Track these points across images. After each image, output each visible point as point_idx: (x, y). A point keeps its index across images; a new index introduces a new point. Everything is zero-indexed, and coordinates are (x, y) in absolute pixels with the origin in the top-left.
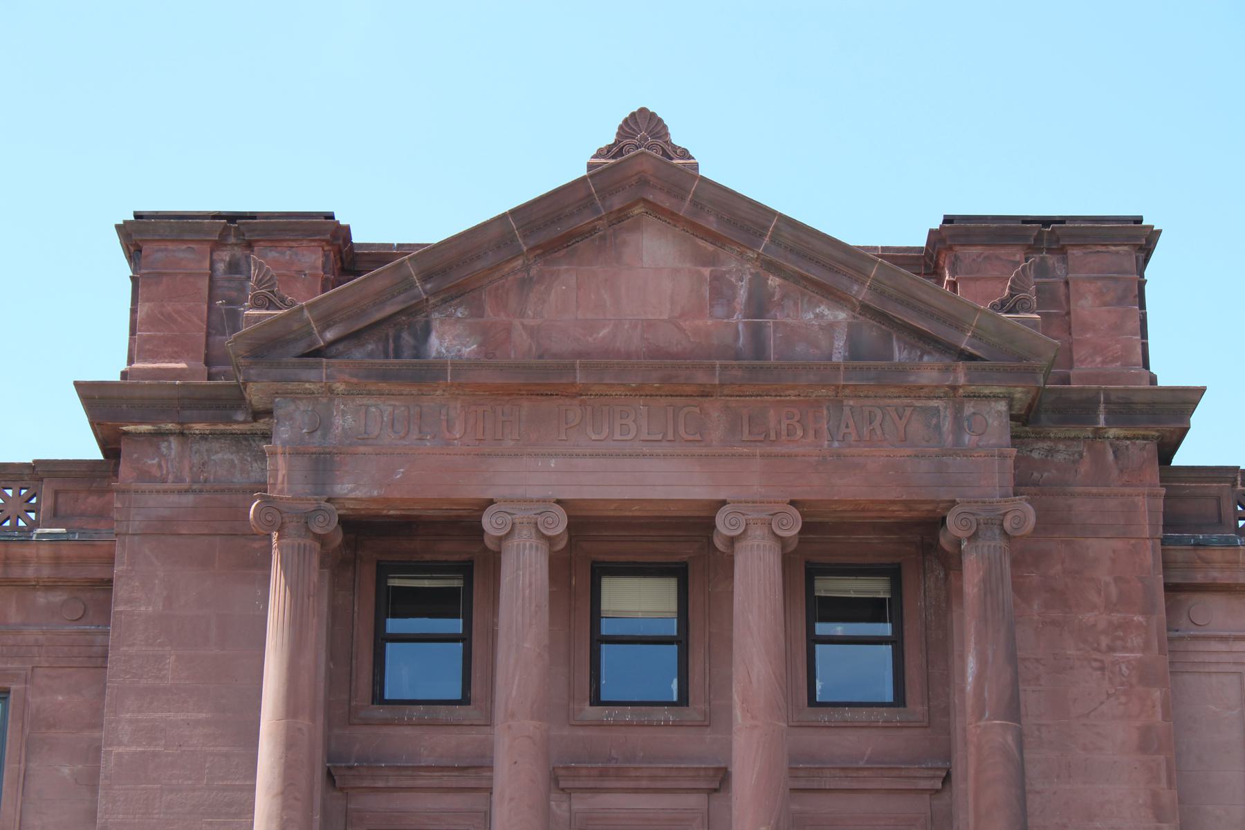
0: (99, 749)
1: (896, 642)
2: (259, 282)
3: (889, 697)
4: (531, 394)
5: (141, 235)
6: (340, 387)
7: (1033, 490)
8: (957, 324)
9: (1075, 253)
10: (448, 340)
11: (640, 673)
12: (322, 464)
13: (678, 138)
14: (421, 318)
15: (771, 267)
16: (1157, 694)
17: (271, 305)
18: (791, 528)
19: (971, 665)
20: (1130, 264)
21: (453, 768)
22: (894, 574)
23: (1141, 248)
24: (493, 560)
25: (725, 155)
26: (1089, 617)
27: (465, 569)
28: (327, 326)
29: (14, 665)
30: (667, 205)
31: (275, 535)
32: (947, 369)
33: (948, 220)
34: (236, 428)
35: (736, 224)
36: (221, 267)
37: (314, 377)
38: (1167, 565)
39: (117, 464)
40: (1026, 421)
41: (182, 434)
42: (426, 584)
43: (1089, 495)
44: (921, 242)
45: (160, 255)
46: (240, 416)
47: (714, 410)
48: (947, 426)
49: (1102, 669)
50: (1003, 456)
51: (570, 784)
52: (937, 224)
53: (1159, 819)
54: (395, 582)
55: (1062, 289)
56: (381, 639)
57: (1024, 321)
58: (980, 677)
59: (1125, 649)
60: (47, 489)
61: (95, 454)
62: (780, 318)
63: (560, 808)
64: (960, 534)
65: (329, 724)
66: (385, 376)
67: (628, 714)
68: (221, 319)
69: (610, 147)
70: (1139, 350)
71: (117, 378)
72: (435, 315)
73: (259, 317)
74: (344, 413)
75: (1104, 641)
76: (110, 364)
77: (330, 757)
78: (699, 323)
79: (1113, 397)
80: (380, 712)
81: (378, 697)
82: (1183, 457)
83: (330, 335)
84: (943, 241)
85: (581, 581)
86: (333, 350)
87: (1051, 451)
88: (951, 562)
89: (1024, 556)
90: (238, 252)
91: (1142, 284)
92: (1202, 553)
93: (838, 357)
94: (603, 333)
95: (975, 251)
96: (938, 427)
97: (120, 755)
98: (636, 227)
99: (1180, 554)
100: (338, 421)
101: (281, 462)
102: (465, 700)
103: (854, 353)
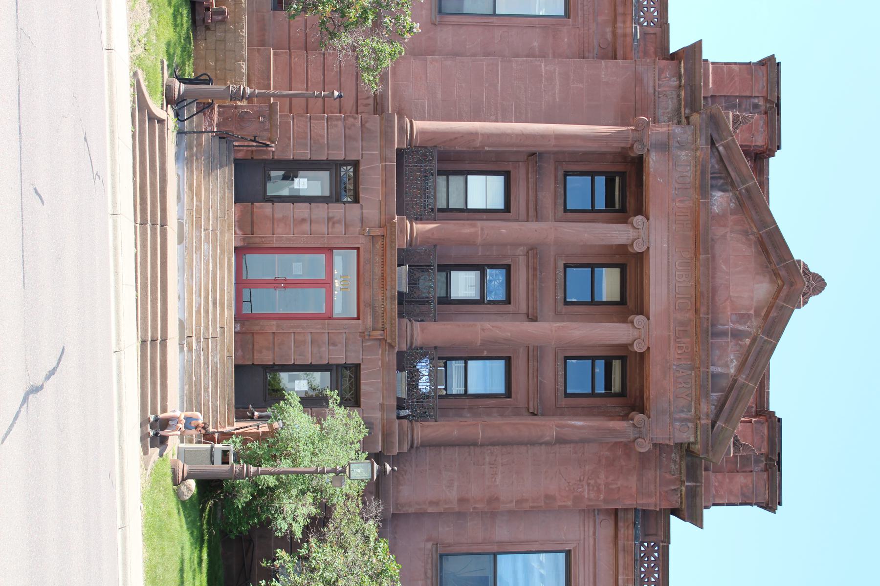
0: (544, 57)
1: (593, 395)
2: (745, 117)
3: (569, 391)
4: (696, 237)
5: (770, 67)
6: (698, 154)
7: (658, 454)
8: (727, 421)
9: (765, 476)
10: (720, 200)
11: (578, 284)
12: (664, 147)
13: (812, 299)
14: (730, 188)
15: (754, 340)
16: (570, 503)
17: (734, 123)
18: (638, 348)
19: (579, 423)
20: (760, 499)
21: (536, 206)
22: (622, 394)
23: (767, 504)
24: (625, 221)
25: (803, 322)
26: (602, 476)
27: (623, 210)
28: (725, 147)
29: (580, 20)
30: (781, 294)
31: (633, 128)
32: (707, 415)
33: (780, 420)
34: (683, 109)
35: (773, 324)
36: (756, 101)
37: (702, 142)
38: (626, 510)
39: (667, 59)
40: (686, 450)
41: (680, 86)
42: (617, 193)
43: (656, 477)
44: (771, 409)
45: (761, 74)
46: (687, 111)
47: (690, 315)
48: (683, 415)
49: (580, 480)
50: (670, 439)
51: (530, 255)
52: (778, 415)
53: (517, 502)
54: (617, 179)
55: (750, 469)
56: (593, 174)
57: (729, 449)
58: (574, 427)
59: (589, 490)
60: (657, 30)
61: (672, 50)
62: (731, 344)
63: (521, 251)
64: (635, 420)
65: (555, 153)
66: (703, 173)
67: (560, 279)
68: (731, 102)
69: (808, 269)
70: (721, 502)
71: (704, 57)
72: (731, 194)
73: (728, 118)
74: (687, 155)
75: (592, 482)
76: (709, 54)
77: (541, 154)
78: (729, 309)
79: (698, 489)
80: (560, 175)
81: (567, 174)
82: (675, 522)
83: (721, 148)
84: (770, 417)
85: (617, 259)
86: (715, 150)
87: (675, 462)
88: (625, 417)
89: (628, 447)
90: (763, 108)
91: (751, 504)
92: (631, 526)
93: (712, 368)
94: (724, 267)
95: (766, 431)
96: (683, 411)
97: (540, 66)
98: (772, 281)
99: (631, 516)
100: (683, 153)
101: (665, 129)
102: (566, 210)
103: (714, 376)
